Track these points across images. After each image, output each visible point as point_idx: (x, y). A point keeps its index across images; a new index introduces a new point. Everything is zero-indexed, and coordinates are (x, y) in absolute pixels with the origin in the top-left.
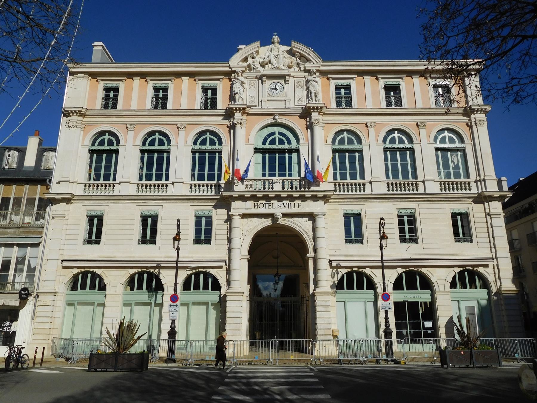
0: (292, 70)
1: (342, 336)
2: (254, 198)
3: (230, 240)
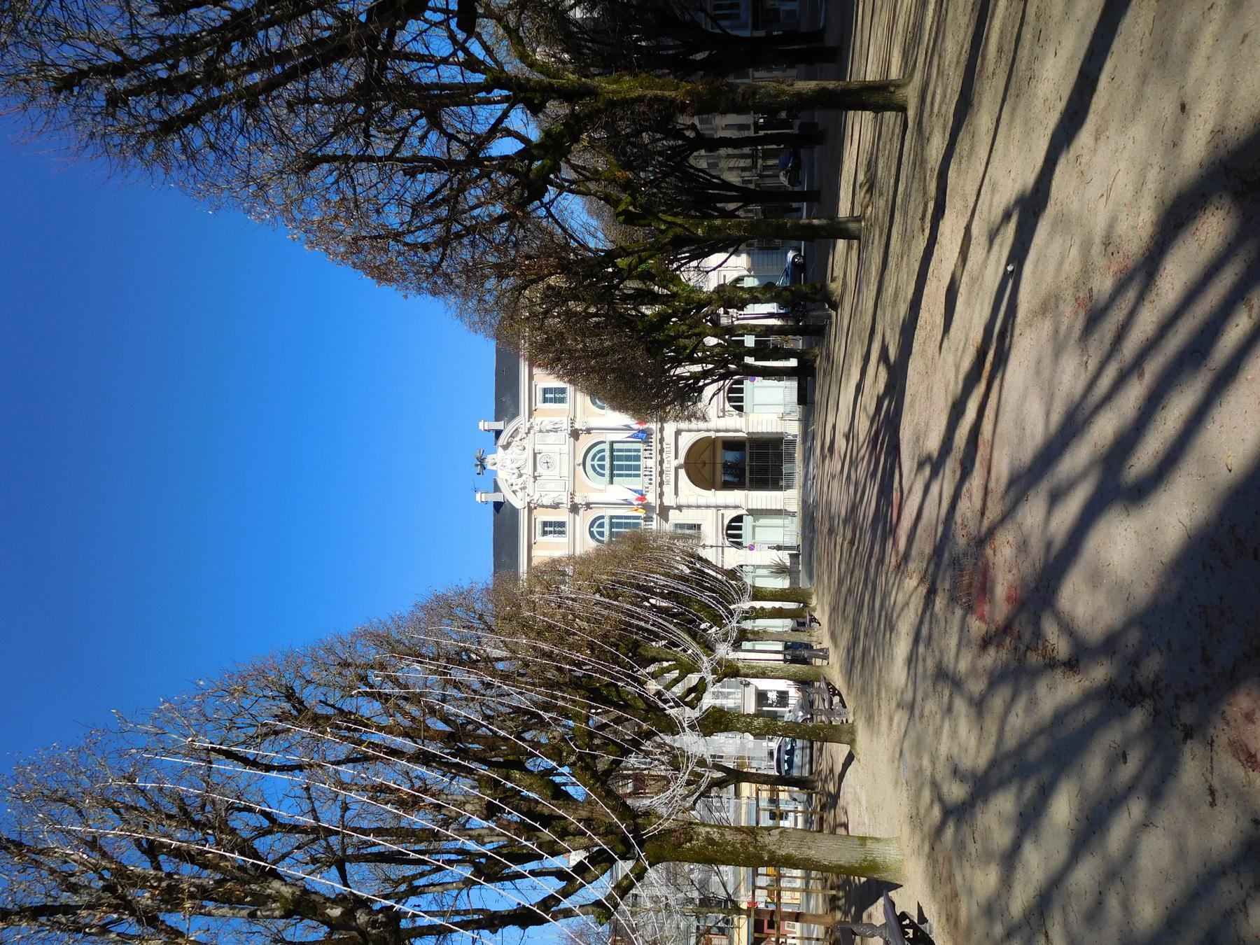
1: (781, 410)
2: (661, 484)
3: (698, 507)
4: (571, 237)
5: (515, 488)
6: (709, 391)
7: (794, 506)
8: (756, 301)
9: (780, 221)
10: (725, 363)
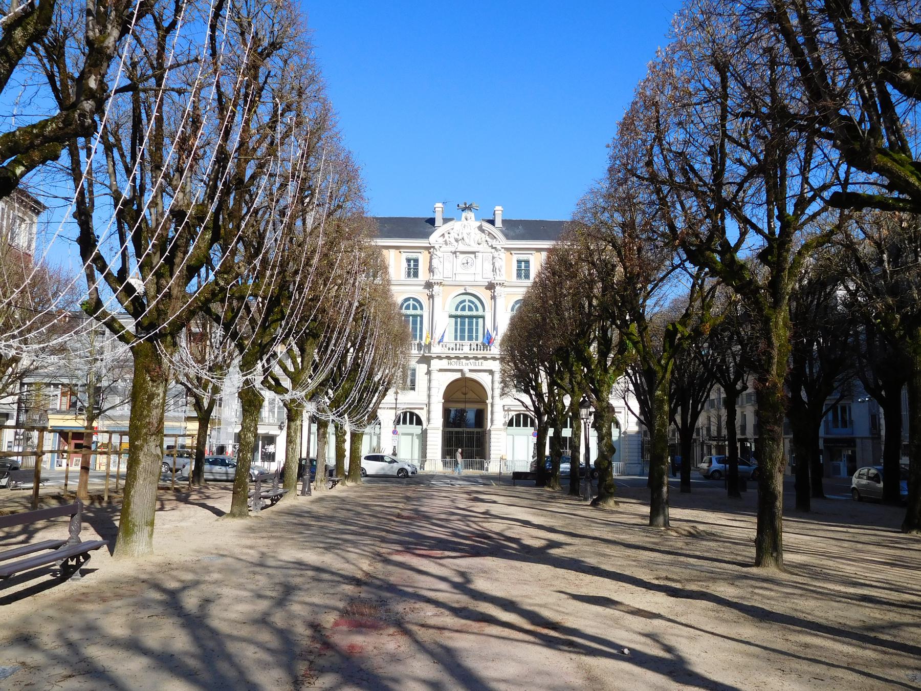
2: (448, 358)
3: (429, 389)
5: (447, 235)
6: (526, 399)
8: (600, 439)
10: (549, 412)
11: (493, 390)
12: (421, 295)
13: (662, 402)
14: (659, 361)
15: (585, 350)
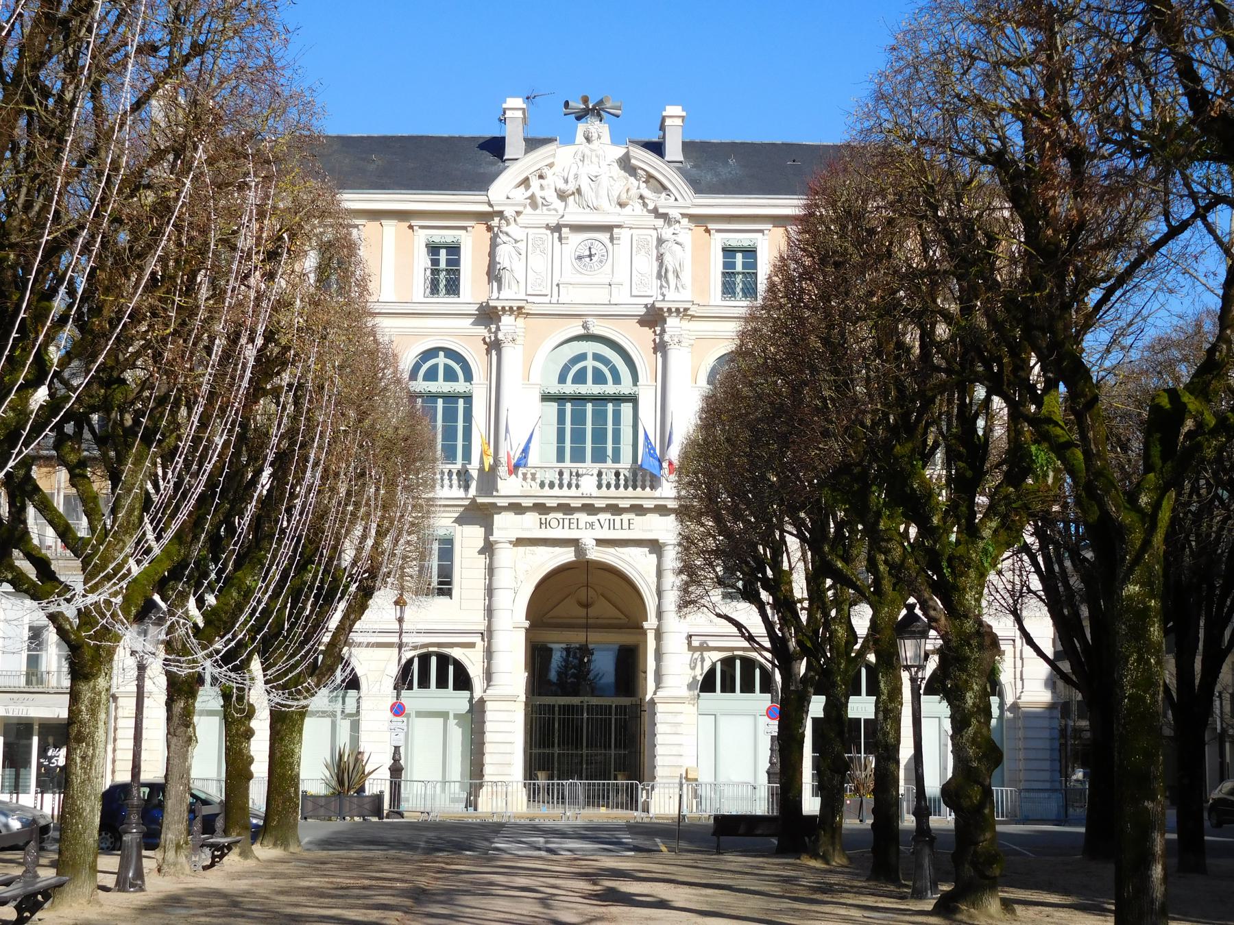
0: (627, 210)
1: (705, 777)
2: (541, 508)
3: (490, 591)
4: (1109, 292)
5: (535, 183)
6: (748, 615)
7: (490, 805)
8: (960, 722)
9: (1159, 785)
10: (811, 650)
11: (660, 593)
12: (465, 337)
13: (1143, 614)
14: (1132, 498)
15: (914, 473)
